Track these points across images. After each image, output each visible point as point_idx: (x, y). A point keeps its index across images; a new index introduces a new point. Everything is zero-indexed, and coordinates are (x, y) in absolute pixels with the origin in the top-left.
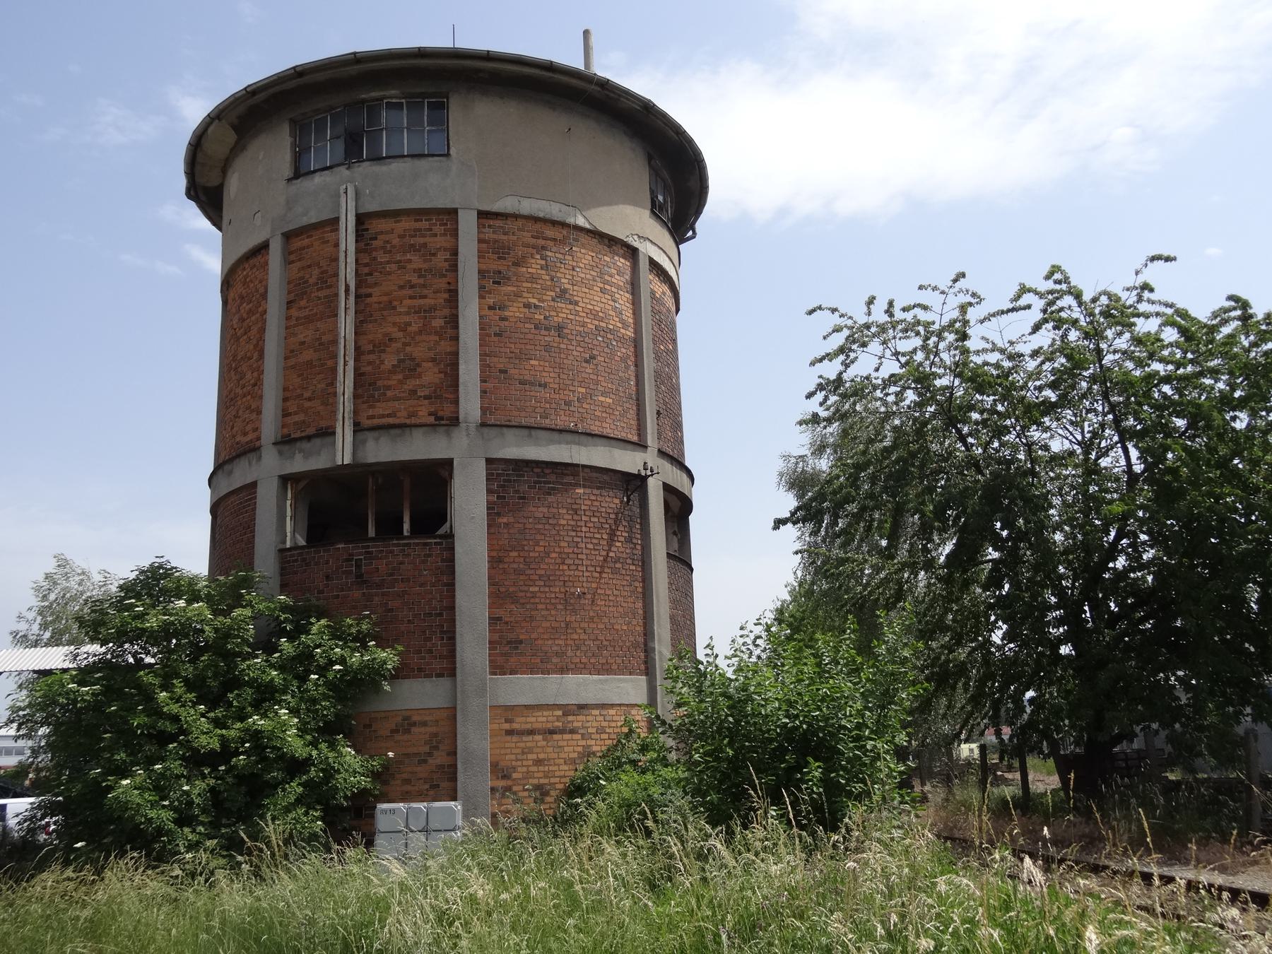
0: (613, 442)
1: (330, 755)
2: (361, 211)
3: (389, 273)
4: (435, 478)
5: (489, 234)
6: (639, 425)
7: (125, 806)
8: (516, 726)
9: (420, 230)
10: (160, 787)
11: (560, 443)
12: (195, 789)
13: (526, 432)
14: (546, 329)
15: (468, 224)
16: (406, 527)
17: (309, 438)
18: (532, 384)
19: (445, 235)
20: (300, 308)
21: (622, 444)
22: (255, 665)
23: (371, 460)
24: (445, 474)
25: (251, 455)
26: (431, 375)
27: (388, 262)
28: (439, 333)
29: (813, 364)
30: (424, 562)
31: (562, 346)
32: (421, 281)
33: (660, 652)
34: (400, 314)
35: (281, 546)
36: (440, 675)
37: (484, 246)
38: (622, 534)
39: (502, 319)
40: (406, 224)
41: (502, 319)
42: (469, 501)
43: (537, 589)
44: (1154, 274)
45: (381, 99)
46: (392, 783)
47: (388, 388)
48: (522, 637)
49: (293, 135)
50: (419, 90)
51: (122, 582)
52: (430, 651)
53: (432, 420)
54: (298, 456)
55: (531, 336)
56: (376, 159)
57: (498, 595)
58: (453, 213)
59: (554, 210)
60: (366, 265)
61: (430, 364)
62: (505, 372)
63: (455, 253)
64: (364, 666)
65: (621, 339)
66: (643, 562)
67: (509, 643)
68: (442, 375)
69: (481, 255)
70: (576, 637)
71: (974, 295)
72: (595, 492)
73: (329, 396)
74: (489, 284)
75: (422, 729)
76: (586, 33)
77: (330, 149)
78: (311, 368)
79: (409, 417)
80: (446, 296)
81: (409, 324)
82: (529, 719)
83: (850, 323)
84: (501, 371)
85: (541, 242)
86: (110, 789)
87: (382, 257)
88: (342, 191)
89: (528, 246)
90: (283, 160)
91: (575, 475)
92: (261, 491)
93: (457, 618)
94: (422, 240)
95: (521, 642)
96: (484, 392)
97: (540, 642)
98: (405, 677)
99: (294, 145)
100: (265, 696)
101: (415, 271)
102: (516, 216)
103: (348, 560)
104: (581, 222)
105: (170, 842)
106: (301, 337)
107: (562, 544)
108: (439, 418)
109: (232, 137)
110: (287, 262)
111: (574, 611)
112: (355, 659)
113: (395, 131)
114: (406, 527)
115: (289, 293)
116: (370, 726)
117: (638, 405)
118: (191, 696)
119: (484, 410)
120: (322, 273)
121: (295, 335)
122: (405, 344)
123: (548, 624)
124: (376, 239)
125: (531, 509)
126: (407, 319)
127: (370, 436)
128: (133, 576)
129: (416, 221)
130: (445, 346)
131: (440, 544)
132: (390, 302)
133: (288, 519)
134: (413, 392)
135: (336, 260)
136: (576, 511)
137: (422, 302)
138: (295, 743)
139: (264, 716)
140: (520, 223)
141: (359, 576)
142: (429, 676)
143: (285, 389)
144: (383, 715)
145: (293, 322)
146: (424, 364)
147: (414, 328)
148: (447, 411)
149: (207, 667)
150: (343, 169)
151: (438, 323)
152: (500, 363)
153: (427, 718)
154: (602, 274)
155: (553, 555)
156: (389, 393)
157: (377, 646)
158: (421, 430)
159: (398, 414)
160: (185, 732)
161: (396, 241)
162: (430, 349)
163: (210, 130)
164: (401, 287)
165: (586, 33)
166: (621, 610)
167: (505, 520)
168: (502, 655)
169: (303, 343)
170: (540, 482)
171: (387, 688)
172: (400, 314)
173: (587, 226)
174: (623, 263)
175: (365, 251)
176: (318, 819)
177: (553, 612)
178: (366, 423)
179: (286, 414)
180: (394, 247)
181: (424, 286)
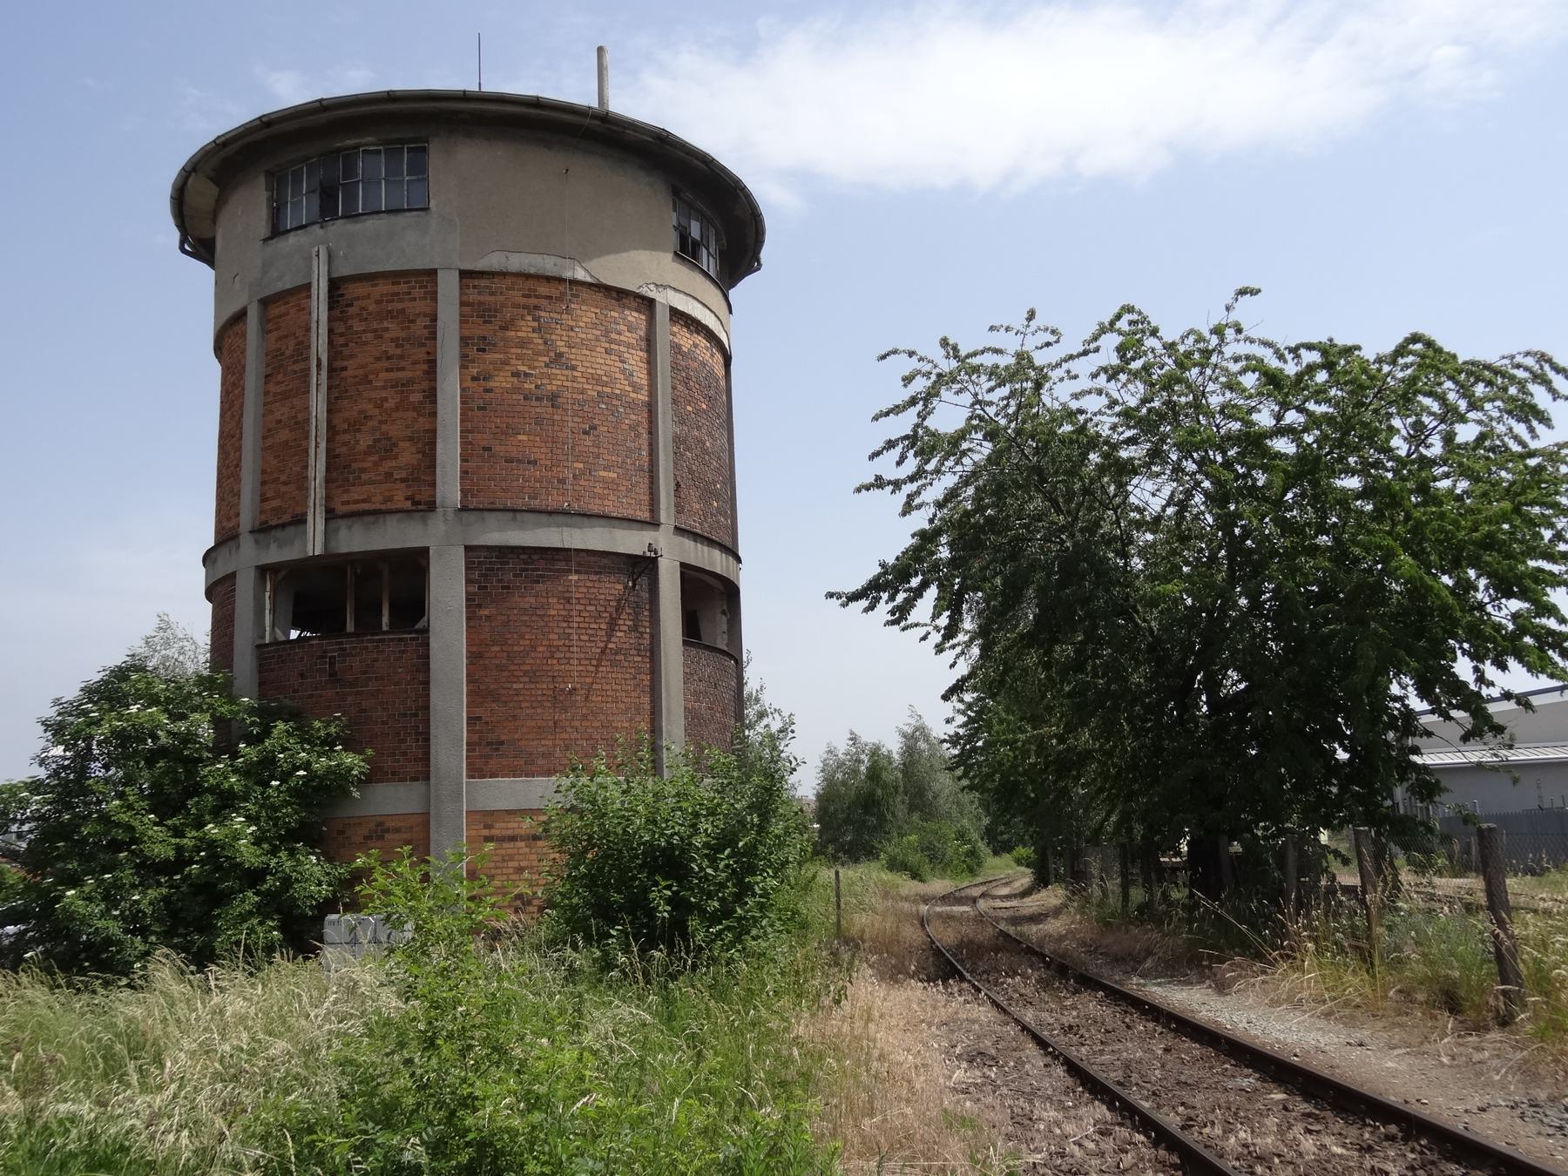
0: (616, 523)
3: (365, 344)
4: (414, 564)
5: (473, 296)
6: (652, 499)
7: (71, 917)
8: (495, 832)
11: (549, 526)
12: (144, 899)
14: (538, 399)
15: (448, 286)
16: (385, 620)
17: (283, 526)
18: (519, 461)
22: (218, 772)
23: (344, 550)
25: (232, 543)
27: (364, 331)
32: (399, 351)
34: (376, 388)
35: (260, 642)
38: (625, 622)
40: (384, 288)
42: (448, 591)
44: (1245, 311)
45: (357, 147)
47: (364, 470)
48: (503, 738)
49: (269, 188)
50: (395, 136)
52: (405, 754)
53: (408, 505)
54: (273, 547)
55: (518, 408)
56: (351, 216)
57: (478, 693)
58: (430, 275)
59: (549, 265)
60: (342, 335)
62: (490, 449)
63: (434, 319)
65: (631, 405)
66: (652, 653)
69: (464, 320)
71: (1053, 332)
73: (302, 482)
74: (472, 352)
75: (396, 836)
76: (600, 50)
77: (303, 206)
78: (284, 448)
79: (385, 501)
80: (425, 367)
81: (386, 399)
83: (927, 367)
84: (485, 449)
85: (533, 301)
86: (58, 899)
87: (358, 326)
89: (516, 306)
91: (568, 560)
92: (239, 581)
94: (400, 306)
95: (502, 743)
96: (464, 472)
99: (270, 200)
100: (226, 802)
101: (392, 340)
102: (504, 274)
104: (581, 275)
105: (118, 952)
106: (278, 415)
107: (552, 636)
109: (213, 190)
110: (265, 332)
114: (385, 620)
116: (343, 832)
117: (651, 477)
121: (271, 412)
122: (381, 422)
123: (533, 724)
124: (351, 305)
126: (383, 394)
127: (343, 523)
128: (98, 677)
135: (309, 330)
136: (568, 600)
137: (400, 374)
138: (248, 853)
140: (509, 281)
141: (333, 674)
142: (403, 780)
143: (263, 472)
146: (401, 444)
147: (391, 404)
148: (424, 497)
149: (165, 773)
150: (316, 228)
151: (415, 397)
152: (483, 439)
154: (607, 332)
156: (364, 477)
157: (345, 750)
158: (395, 517)
160: (134, 841)
162: (407, 427)
164: (378, 359)
165: (600, 50)
166: (622, 706)
167: (486, 612)
168: (481, 757)
169: (280, 421)
172: (376, 388)
173: (589, 279)
174: (636, 317)
175: (341, 319)
176: (274, 928)
179: (264, 499)
181: (401, 357)
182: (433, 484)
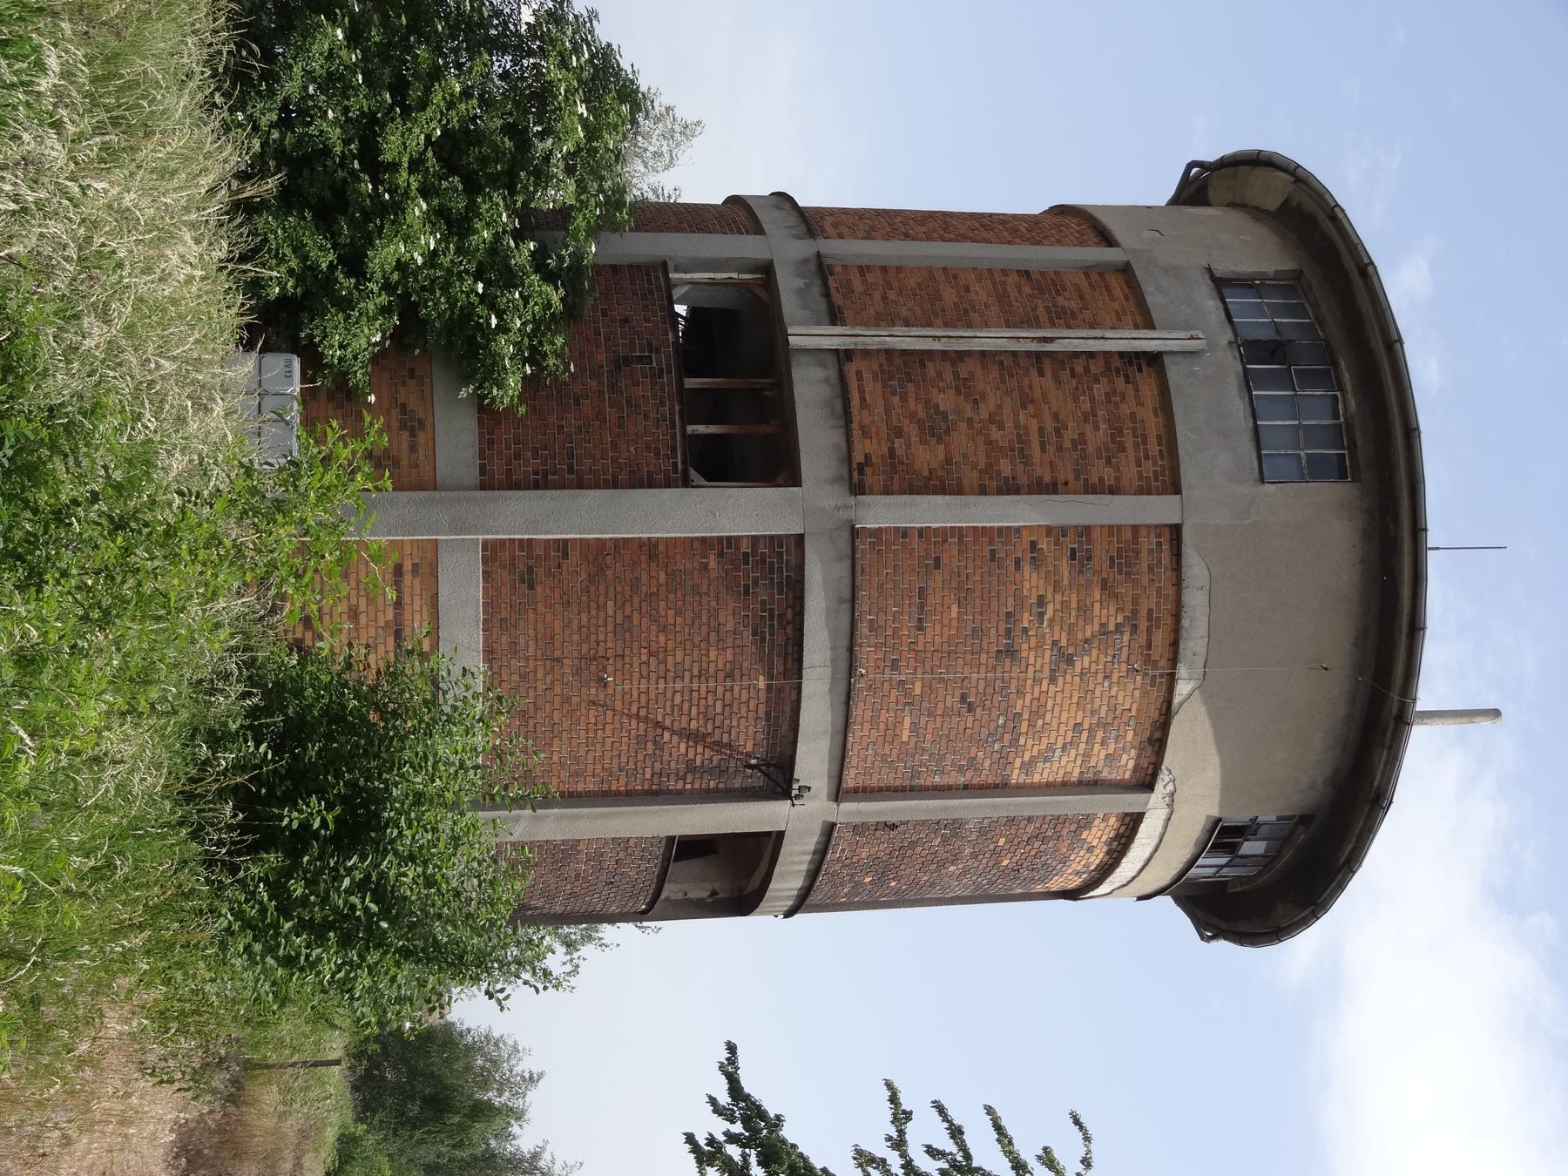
0: (840, 738)
1: (371, 306)
2: (1167, 360)
4: (777, 465)
5: (1147, 543)
6: (872, 790)
7: (308, 34)
8: (408, 578)
9: (1145, 442)
10: (333, 82)
11: (833, 648)
12: (329, 126)
13: (847, 594)
14: (1008, 631)
15: (1158, 510)
16: (701, 429)
17: (827, 295)
18: (921, 607)
19: (1140, 479)
20: (1019, 286)
21: (838, 753)
24: (780, 479)
25: (803, 228)
26: (925, 457)
27: (1092, 398)
28: (988, 470)
29: (989, 1110)
30: (648, 447)
31: (984, 657)
32: (1067, 444)
33: (518, 819)
35: (671, 265)
36: (483, 470)
37: (1128, 535)
38: (700, 755)
39: (1018, 562)
40: (1153, 425)
41: (1018, 562)
42: (741, 512)
43: (610, 612)
45: (1341, 388)
46: (331, 405)
47: (904, 398)
48: (539, 588)
49: (1279, 275)
51: (615, 47)
52: (518, 456)
54: (800, 283)
55: (994, 604)
56: (1248, 381)
57: (600, 554)
59: (1195, 643)
60: (1087, 369)
61: (942, 457)
64: (497, 358)
65: (1003, 761)
66: (656, 793)
67: (530, 569)
68: (926, 473)
69: (1113, 530)
70: (540, 674)
72: (762, 709)
73: (887, 318)
74: (1069, 543)
75: (405, 446)
77: (1259, 319)
78: (933, 296)
79: (862, 428)
80: (1047, 479)
81: (1001, 427)
82: (417, 598)
84: (937, 561)
85: (1143, 624)
87: (1099, 390)
88: (1194, 333)
89: (1135, 602)
90: (1244, 264)
91: (785, 674)
92: (752, 240)
93: (566, 492)
94: (1129, 445)
95: (531, 587)
96: (905, 533)
97: (532, 617)
98: (481, 422)
99: (1264, 277)
100: (456, 225)
102: (1178, 584)
103: (650, 345)
104: (1183, 689)
106: (975, 287)
107: (679, 654)
108: (861, 472)
109: (1273, 204)
110: (1087, 270)
111: (577, 672)
112: (505, 347)
113: (1294, 407)
114: (701, 429)
115: (1042, 273)
118: (455, 123)
119: (878, 532)
120: (1073, 313)
121: (980, 280)
123: (558, 629)
124: (1128, 382)
125: (732, 605)
126: (1009, 424)
127: (832, 372)
129: (1159, 437)
130: (971, 477)
131: (675, 471)
132: (1032, 401)
133: (711, 275)
134: (899, 433)
135: (1092, 326)
137: (1036, 446)
138: (385, 255)
139: (427, 217)
141: (627, 361)
143: (899, 269)
144: (427, 394)
145: (998, 278)
147: (995, 434)
148: (870, 479)
150: (1229, 335)
151: (1005, 467)
152: (950, 556)
153: (421, 451)
155: (662, 639)
156: (896, 400)
159: (865, 412)
160: (406, 112)
161: (1125, 409)
162: (965, 456)
163: (1281, 174)
164: (1056, 416)
165: (1495, 713)
166: (582, 752)
167: (713, 564)
169: (967, 289)
170: (771, 617)
171: (463, 393)
172: (1016, 415)
173: (1177, 700)
174: (1126, 765)
175: (1108, 369)
176: (283, 288)
177: (576, 637)
178: (851, 370)
179: (863, 270)
180: (1117, 405)
181: (1060, 448)
182: (887, 491)
